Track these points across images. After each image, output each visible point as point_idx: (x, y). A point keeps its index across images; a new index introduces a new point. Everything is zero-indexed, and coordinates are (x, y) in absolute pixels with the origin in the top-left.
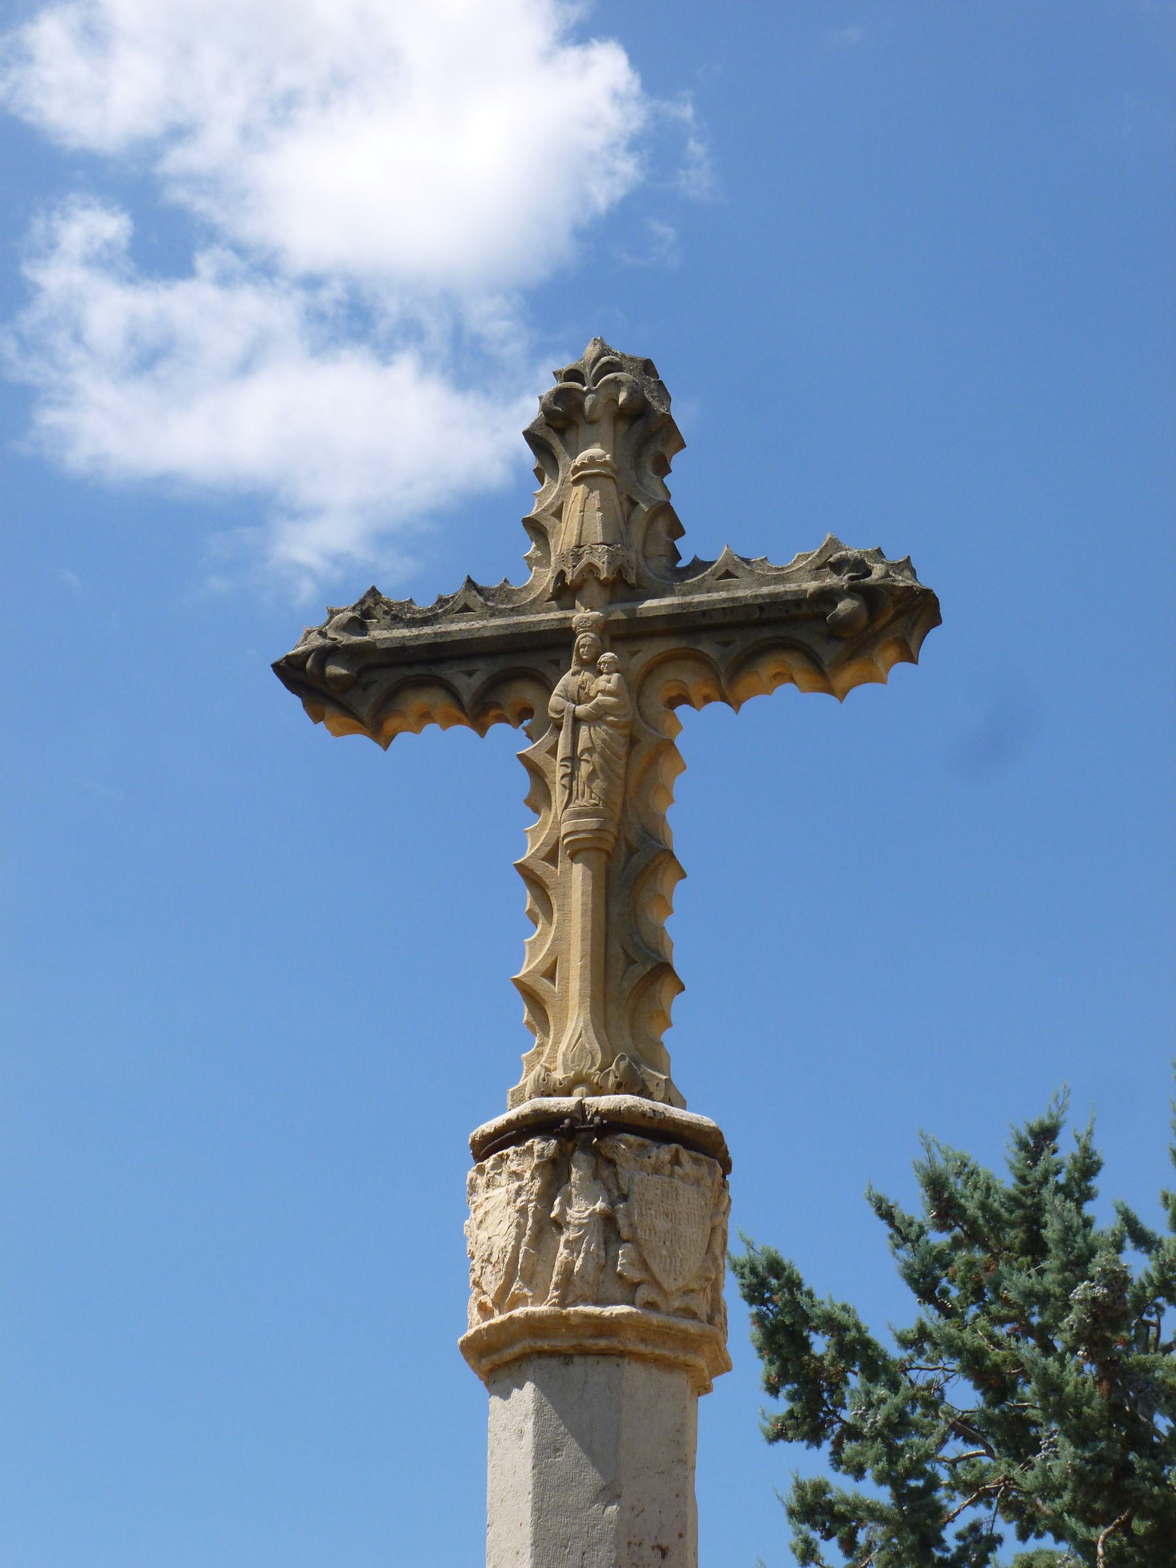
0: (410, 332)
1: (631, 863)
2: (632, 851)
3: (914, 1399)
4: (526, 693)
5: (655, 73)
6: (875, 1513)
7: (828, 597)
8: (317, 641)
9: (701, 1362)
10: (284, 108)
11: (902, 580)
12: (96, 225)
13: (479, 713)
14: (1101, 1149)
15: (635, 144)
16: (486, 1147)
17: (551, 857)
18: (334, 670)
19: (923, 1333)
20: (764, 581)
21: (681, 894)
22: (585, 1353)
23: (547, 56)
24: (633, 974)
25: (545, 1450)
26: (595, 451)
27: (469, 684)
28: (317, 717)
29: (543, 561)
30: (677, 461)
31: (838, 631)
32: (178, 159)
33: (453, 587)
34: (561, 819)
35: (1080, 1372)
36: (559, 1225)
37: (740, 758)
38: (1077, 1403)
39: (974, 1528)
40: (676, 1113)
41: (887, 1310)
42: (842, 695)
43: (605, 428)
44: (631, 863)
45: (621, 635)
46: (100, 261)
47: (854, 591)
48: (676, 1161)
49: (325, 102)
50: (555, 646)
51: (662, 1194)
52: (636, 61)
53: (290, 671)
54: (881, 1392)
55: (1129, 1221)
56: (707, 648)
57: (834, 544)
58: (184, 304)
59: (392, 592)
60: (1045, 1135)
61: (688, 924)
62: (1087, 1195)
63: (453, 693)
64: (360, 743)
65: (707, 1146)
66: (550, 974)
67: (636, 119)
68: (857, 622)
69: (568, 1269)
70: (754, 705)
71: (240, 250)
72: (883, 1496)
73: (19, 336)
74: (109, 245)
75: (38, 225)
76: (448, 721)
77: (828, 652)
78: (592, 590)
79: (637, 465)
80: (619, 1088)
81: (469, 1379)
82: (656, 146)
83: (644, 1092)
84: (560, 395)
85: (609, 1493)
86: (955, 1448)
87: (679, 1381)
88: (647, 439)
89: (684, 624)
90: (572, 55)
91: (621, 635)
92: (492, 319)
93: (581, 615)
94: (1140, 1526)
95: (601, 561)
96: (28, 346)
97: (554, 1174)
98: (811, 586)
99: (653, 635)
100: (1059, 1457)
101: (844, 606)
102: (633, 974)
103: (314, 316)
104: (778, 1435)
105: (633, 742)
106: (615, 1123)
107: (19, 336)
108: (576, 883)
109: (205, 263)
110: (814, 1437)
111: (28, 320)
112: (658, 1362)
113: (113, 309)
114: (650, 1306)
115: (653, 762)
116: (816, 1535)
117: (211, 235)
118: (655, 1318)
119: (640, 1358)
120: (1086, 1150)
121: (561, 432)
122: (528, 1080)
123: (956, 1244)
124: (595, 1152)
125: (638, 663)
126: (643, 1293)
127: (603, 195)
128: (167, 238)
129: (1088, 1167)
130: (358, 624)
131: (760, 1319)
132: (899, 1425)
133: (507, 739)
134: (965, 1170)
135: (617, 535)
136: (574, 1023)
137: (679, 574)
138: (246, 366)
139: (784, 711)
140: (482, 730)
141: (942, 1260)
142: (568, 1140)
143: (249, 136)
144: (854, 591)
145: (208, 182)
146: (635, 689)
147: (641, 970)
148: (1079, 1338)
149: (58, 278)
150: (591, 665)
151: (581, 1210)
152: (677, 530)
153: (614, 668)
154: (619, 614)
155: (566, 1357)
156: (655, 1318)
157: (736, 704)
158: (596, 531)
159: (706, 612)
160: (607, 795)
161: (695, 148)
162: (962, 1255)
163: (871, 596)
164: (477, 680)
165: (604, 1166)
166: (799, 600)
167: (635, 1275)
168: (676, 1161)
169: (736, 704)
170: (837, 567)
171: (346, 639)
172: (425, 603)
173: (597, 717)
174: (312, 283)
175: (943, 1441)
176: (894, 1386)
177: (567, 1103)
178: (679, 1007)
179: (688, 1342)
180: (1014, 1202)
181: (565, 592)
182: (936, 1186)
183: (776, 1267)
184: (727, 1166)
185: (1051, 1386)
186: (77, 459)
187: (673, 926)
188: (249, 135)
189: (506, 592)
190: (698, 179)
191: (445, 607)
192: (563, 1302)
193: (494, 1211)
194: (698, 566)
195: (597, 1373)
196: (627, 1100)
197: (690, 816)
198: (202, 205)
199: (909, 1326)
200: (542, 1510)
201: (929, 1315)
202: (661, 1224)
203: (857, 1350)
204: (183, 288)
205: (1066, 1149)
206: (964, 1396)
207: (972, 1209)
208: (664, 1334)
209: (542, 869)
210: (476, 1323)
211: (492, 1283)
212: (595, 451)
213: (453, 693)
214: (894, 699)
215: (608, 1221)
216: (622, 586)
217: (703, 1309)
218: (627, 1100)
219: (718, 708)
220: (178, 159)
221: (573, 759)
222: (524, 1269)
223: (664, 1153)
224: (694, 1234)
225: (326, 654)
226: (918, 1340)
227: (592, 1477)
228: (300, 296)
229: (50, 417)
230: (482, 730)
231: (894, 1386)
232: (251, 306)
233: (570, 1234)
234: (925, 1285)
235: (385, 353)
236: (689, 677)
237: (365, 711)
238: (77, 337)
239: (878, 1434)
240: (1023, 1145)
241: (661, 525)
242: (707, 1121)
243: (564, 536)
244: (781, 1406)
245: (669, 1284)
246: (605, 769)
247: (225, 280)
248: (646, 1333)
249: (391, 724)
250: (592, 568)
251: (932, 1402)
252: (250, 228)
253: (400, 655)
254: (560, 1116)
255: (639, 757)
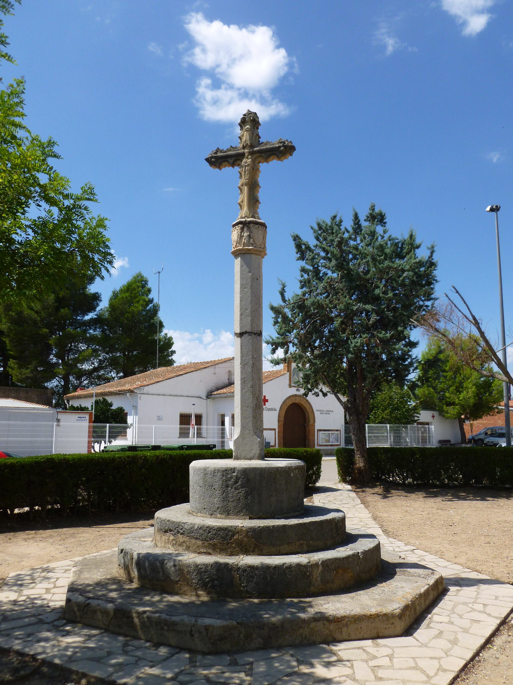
0: (254, 96)
1: (253, 186)
2: (253, 184)
3: (316, 255)
4: (239, 162)
5: (290, 53)
6: (310, 271)
7: (280, 147)
8: (210, 156)
9: (262, 254)
10: (233, 61)
11: (290, 144)
12: (206, 81)
13: (233, 165)
14: (343, 219)
15: (287, 65)
16: (234, 226)
17: (242, 185)
18: (213, 160)
19: (317, 245)
20: (271, 145)
21: (260, 190)
22: (246, 253)
23: (273, 51)
24: (253, 201)
25: (241, 266)
26: (248, 126)
27: (231, 161)
28: (211, 166)
29: (241, 143)
30: (260, 127)
31: (281, 152)
32: (218, 70)
33: (229, 147)
34: (244, 180)
35: (336, 251)
36: (243, 236)
37: (268, 170)
38: (336, 255)
39: (324, 272)
40: (259, 221)
41: (312, 242)
42: (282, 161)
43: (249, 123)
44: (253, 186)
45: (252, 153)
46: (207, 87)
47: (283, 146)
48: (259, 227)
49: (240, 60)
50: (242, 155)
51: (257, 232)
52: (287, 51)
53: (207, 160)
54: (311, 254)
55: (346, 229)
56: (263, 155)
57: (281, 139)
58: (220, 93)
59: (221, 148)
60: (335, 217)
61: (261, 195)
62: (341, 225)
63: (229, 162)
64: (217, 170)
65: (263, 225)
66: (242, 202)
67: (286, 61)
68: (284, 150)
69: (244, 242)
70: (270, 163)
71: (228, 84)
72: (311, 268)
73: (196, 99)
74: (208, 84)
75: (198, 82)
76: (229, 167)
77: (280, 155)
78: (248, 147)
79: (254, 129)
80: (251, 217)
81: (232, 257)
82: (290, 65)
83: (255, 218)
84: (243, 118)
85: (250, 272)
86: (322, 261)
87: (259, 257)
88: (255, 124)
89: (260, 152)
90: (277, 50)
91: (252, 153)
92: (266, 94)
93: (246, 151)
94: (345, 272)
95: (249, 143)
96: (197, 101)
97: (242, 229)
98: (277, 145)
99: (256, 153)
100: (334, 262)
101: (282, 148)
102: (253, 201)
103: (240, 94)
104: (298, 260)
105: (253, 169)
106: (250, 222)
107: (196, 99)
108: (246, 189)
109: (223, 87)
110: (303, 260)
111: (197, 97)
112: (256, 254)
113: (209, 95)
114: (255, 247)
115: (256, 172)
116: (303, 274)
117: (224, 82)
118: (255, 248)
119: (254, 254)
120: (341, 219)
121: (243, 124)
122: (239, 217)
123: (322, 233)
124: (247, 226)
125: (254, 157)
126: (254, 245)
127: (282, 73)
128: (217, 83)
129: (341, 221)
130: (216, 153)
131: (295, 243)
132: (313, 258)
133: (237, 169)
134: (324, 222)
135: (251, 138)
136: (245, 208)
137: (259, 144)
138: (230, 103)
139: (274, 163)
140: (233, 167)
141: (320, 235)
142: (244, 225)
143: (229, 66)
144: (283, 146)
145: (223, 74)
146: (253, 161)
147: (254, 201)
148: (336, 246)
149: (201, 90)
150: (247, 158)
151: (246, 234)
152: (260, 137)
153: (250, 158)
154: (251, 150)
155: (244, 254)
156: (255, 248)
157: (268, 163)
158: (248, 139)
159: (263, 150)
160: (249, 177)
161: (296, 65)
162: (323, 234)
163: (285, 147)
164: (232, 160)
165: (249, 228)
166: (276, 148)
167: (253, 243)
168: (259, 227)
169: (268, 163)
170: (281, 143)
171: (214, 155)
172: (225, 149)
173: (248, 165)
174: (239, 89)
175: (320, 260)
176: (313, 253)
177: (244, 220)
178: (260, 206)
179: (260, 251)
180: (330, 227)
181: (244, 147)
182: (319, 225)
183: (297, 236)
184: (266, 227)
185: (332, 253)
186: (206, 118)
187: (259, 195)
188: (229, 66)
189: (236, 148)
190: (296, 70)
191: (228, 150)
192: (243, 247)
193: (235, 234)
194: (262, 143)
195: (248, 256)
196: (252, 219)
197: (261, 179)
198: (222, 77)
199: (315, 244)
200: (241, 274)
201: (318, 243)
202: (256, 236)
203: (308, 248)
204: (220, 91)
205: (338, 219)
206: (323, 254)
207: (324, 228)
208: (257, 250)
209: (241, 187)
210: (233, 250)
211: (235, 244)
212: (248, 126)
213: (229, 162)
214: (289, 161)
215: (249, 235)
216: (252, 146)
217: (263, 247)
218: (252, 219)
219: (265, 163)
220: (218, 70)
221: (245, 172)
222: (239, 242)
223: (257, 226)
224: (261, 237)
225: (212, 157)
226: (316, 246)
227: (248, 270)
228: (237, 91)
229: (201, 112)
230: (233, 167)
231: (313, 253)
232: (231, 94)
233: (244, 238)
234: (317, 239)
235: (250, 100)
236: (260, 159)
237: (217, 166)
238: (204, 99)
239: (310, 260)
240: (332, 218)
241: (257, 137)
242: (263, 222)
243: (244, 139)
244: (298, 255)
245: (258, 244)
246: (249, 173)
247: (226, 89)
248: (255, 250)
249: (221, 167)
250: (247, 144)
251: (318, 255)
252: (229, 81)
253: (222, 157)
254: (243, 222)
255: (254, 171)
